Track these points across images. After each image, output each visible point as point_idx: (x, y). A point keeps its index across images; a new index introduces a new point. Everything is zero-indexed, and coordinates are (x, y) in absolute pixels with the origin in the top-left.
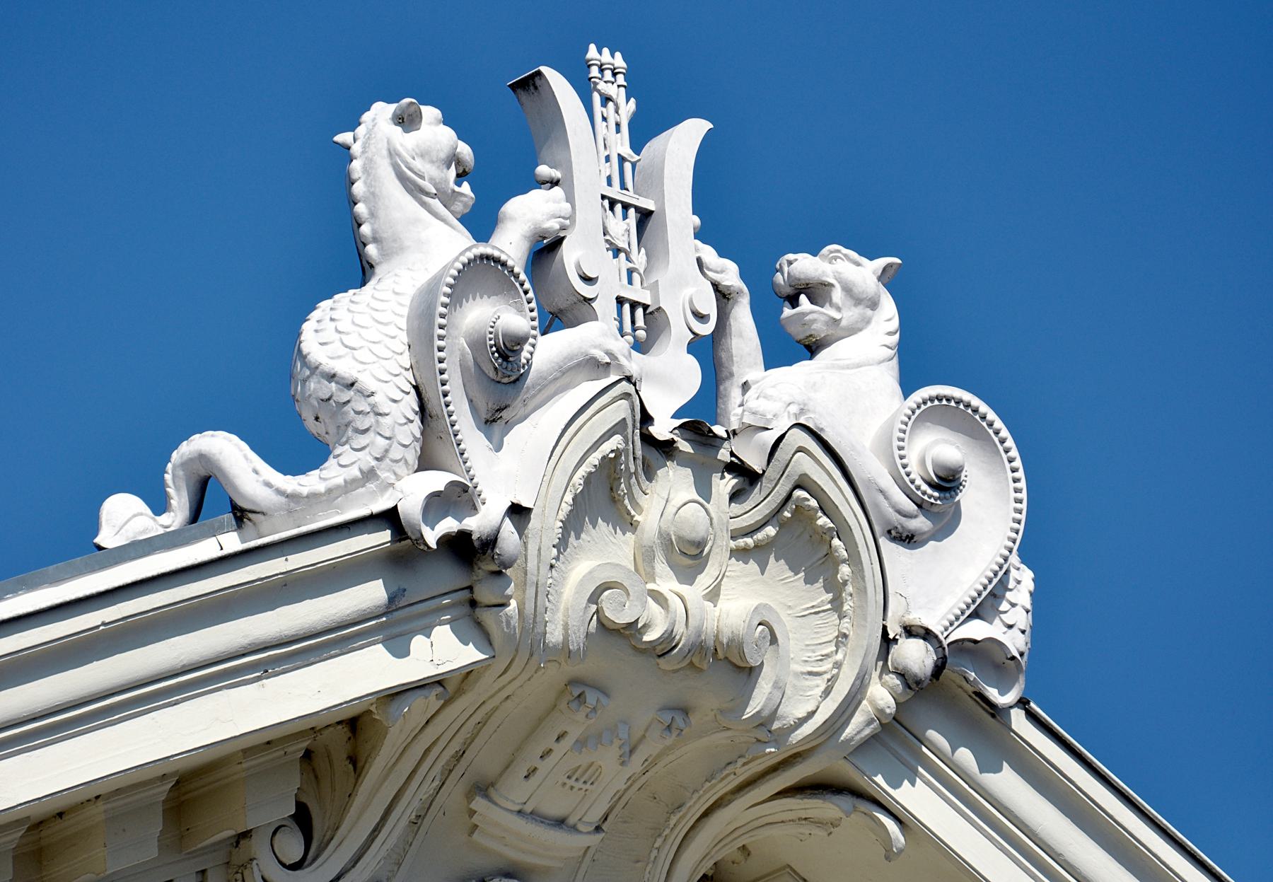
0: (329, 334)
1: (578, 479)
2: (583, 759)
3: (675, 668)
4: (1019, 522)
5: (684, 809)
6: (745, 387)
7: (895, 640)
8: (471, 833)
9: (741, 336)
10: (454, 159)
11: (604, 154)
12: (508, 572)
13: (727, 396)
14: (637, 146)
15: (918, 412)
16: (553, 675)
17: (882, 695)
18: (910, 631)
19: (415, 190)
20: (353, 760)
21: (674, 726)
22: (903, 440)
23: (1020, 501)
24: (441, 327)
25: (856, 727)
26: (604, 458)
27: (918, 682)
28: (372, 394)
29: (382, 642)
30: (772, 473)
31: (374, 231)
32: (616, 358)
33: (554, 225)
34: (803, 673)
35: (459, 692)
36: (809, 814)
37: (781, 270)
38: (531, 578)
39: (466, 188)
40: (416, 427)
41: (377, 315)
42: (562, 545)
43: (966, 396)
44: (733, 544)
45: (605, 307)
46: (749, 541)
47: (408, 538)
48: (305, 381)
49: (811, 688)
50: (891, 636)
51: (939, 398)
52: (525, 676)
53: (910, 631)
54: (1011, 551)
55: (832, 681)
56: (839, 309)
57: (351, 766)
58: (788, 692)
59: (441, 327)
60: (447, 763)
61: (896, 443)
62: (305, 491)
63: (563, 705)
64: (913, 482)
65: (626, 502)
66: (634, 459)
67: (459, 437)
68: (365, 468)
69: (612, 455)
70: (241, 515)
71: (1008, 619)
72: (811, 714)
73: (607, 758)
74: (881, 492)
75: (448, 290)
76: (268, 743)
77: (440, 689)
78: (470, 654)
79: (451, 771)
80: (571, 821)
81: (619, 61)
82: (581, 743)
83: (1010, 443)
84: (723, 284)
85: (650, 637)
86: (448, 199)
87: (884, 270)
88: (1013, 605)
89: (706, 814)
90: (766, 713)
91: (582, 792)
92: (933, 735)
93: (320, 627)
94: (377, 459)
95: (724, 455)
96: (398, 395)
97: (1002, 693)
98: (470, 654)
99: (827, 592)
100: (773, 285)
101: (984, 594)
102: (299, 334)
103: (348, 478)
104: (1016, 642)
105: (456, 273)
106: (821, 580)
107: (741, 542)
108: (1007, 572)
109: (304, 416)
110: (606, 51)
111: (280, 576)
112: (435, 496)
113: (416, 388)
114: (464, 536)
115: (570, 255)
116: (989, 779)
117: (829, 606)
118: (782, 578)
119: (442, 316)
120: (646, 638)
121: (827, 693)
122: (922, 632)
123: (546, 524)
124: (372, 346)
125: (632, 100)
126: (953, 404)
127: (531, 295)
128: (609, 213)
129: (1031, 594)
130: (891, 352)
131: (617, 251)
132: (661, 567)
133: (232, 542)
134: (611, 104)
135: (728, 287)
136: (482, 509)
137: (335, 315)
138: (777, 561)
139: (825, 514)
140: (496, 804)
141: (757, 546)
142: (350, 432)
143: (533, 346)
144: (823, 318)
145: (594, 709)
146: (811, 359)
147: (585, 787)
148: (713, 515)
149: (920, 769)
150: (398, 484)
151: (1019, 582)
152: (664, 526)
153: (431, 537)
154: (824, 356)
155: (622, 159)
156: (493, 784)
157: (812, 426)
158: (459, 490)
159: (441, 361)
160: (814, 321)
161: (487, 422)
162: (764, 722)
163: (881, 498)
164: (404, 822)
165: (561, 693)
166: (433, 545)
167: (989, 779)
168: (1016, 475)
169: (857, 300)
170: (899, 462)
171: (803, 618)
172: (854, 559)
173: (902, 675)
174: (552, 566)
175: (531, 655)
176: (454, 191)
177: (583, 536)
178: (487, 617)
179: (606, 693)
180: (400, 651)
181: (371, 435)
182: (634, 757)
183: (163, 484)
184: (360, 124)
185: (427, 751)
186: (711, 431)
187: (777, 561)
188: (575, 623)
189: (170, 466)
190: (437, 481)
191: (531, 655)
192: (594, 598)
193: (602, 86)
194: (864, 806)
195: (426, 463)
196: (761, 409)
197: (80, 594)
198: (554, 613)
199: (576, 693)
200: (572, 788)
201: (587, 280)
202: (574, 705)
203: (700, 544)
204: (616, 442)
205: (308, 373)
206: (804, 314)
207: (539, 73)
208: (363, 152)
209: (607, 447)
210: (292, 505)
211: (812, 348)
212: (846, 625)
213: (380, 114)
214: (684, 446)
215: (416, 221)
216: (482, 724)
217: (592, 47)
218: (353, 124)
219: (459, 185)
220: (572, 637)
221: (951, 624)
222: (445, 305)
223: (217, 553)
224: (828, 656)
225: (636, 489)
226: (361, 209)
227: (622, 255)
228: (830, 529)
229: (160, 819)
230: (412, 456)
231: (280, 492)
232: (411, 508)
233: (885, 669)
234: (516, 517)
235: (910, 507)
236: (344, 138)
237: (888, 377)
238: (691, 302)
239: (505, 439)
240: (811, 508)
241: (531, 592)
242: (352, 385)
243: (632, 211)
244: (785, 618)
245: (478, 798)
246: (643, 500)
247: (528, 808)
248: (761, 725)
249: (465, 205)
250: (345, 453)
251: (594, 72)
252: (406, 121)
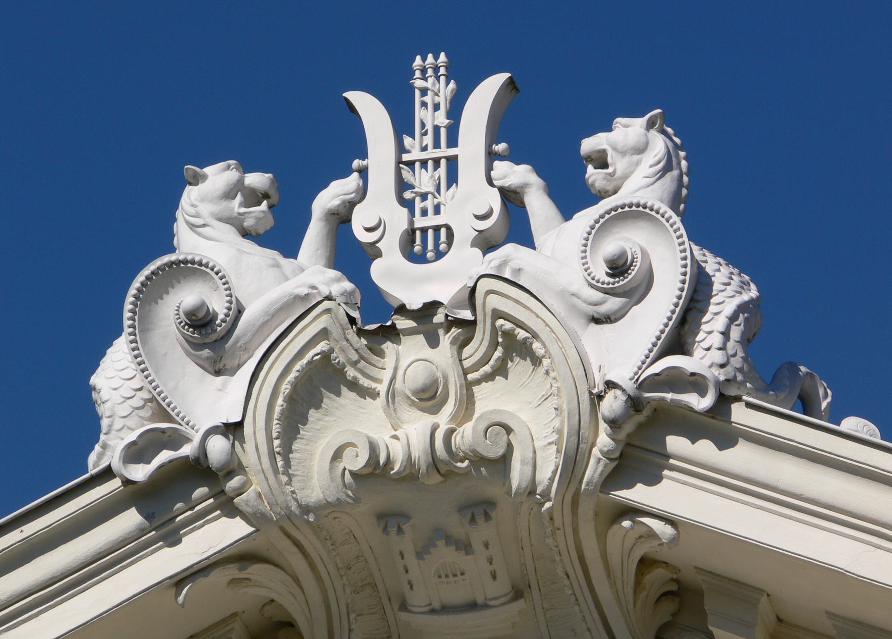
25: (594, 470)
30: (480, 317)
34: (545, 446)
74: (574, 295)
84: (506, 185)
111: (17, 544)
118: (521, 384)
163: (575, 299)
169: (622, 153)
171: (540, 406)
188: (324, 483)
235: (599, 296)
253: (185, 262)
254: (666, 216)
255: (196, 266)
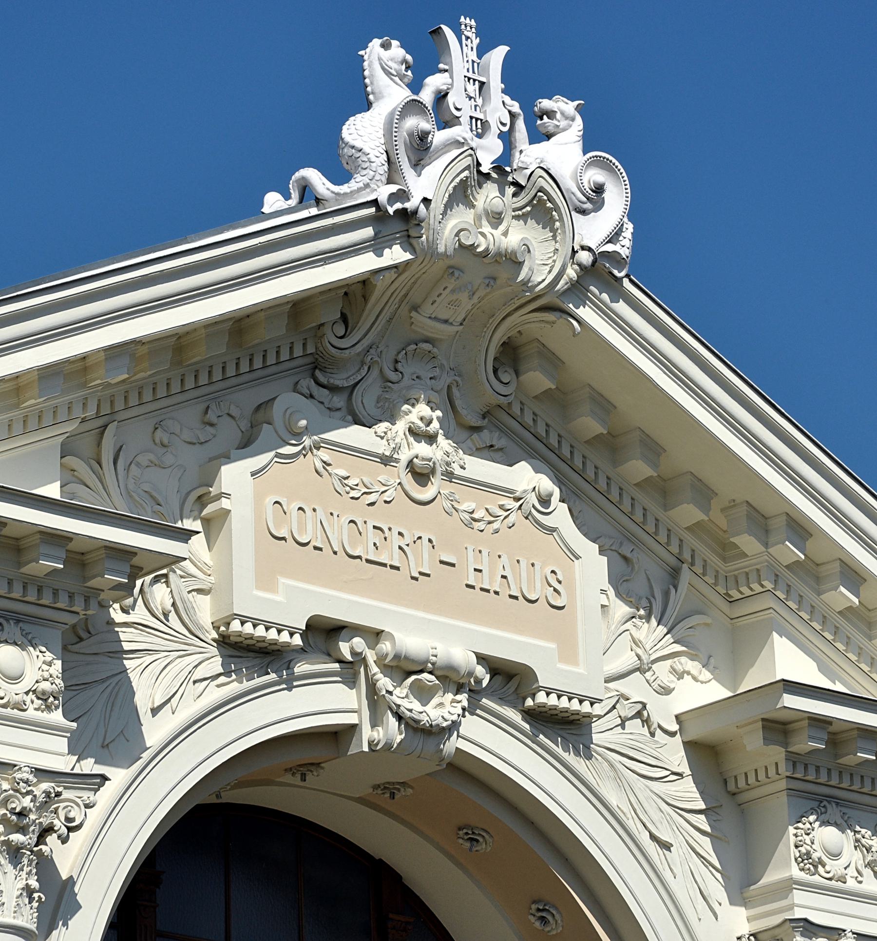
0: (352, 130)
1: (451, 188)
2: (454, 297)
3: (490, 262)
4: (627, 205)
5: (495, 317)
6: (521, 152)
7: (577, 252)
8: (411, 325)
9: (519, 131)
10: (404, 61)
11: (466, 59)
12: (423, 224)
13: (514, 155)
14: (480, 56)
15: (588, 162)
16: (441, 265)
17: (571, 273)
18: (583, 248)
19: (388, 74)
20: (364, 297)
21: (490, 285)
22: (581, 173)
23: (628, 197)
24: (396, 128)
25: (561, 285)
26: (461, 180)
27: (586, 268)
28: (368, 154)
29: (373, 251)
30: (529, 186)
31: (372, 90)
32: (467, 141)
33: (445, 87)
34: (541, 264)
35: (404, 271)
36: (544, 319)
37: (537, 106)
38: (432, 227)
39: (409, 73)
40: (386, 167)
41: (372, 123)
42: (444, 214)
43: (607, 156)
44: (513, 214)
45: (465, 120)
46: (520, 213)
47: (382, 211)
48: (343, 149)
49: (544, 270)
50: (575, 250)
51: (596, 157)
52: (429, 265)
53: (583, 248)
54: (623, 217)
55: (552, 267)
56: (559, 121)
57: (363, 299)
58: (535, 272)
59: (396, 128)
60: (401, 298)
61: (579, 174)
62: (342, 192)
63: (446, 276)
64: (585, 189)
65: (471, 197)
66: (474, 180)
67: (403, 171)
68: (365, 183)
69: (465, 179)
70: (318, 201)
71: (622, 243)
72: (544, 280)
73: (464, 297)
75: (399, 113)
76: (330, 290)
77: (396, 270)
78: (408, 256)
79: (403, 301)
80: (451, 321)
81: (473, 23)
82: (453, 291)
83: (624, 174)
85: (479, 250)
86: (402, 77)
87: (578, 106)
88: (625, 238)
89: (504, 319)
90: (525, 280)
91: (454, 310)
92: (592, 288)
93: (346, 245)
94: (370, 180)
95: (510, 179)
96: (379, 155)
97: (619, 272)
98: (408, 256)
99: (551, 232)
100: (534, 112)
101: (613, 234)
102: (342, 130)
103: (359, 187)
104: (625, 252)
105: (402, 107)
106: (548, 228)
107: (517, 213)
108: (622, 225)
109: (343, 162)
110: (468, 19)
112: (393, 194)
113: (386, 152)
114: (405, 210)
115: (451, 99)
116: (614, 305)
117: (551, 238)
119: (396, 123)
120: (478, 250)
121: (550, 272)
122: (588, 248)
123: (438, 206)
124: (369, 135)
125: (478, 38)
126: (602, 159)
127: (432, 115)
128: (468, 83)
129: (632, 233)
130: (579, 138)
131: (470, 98)
132: (485, 222)
133: (314, 211)
134: (469, 40)
135: (514, 112)
136: (412, 200)
137: (355, 123)
138: (531, 220)
139: (550, 202)
140: (420, 314)
141: (523, 214)
142: (360, 169)
143: (433, 135)
144: (552, 125)
145: (458, 278)
146: (548, 141)
147: (455, 308)
148: (505, 202)
149: (587, 302)
150: (378, 190)
151: (627, 229)
152: (486, 207)
153: (391, 210)
154: (553, 139)
155: (473, 62)
156: (419, 307)
157: (545, 167)
158: (402, 192)
159: (396, 141)
160: (549, 126)
161: (414, 165)
162: (525, 283)
163: (573, 196)
164: (384, 321)
165: (445, 271)
166: (392, 214)
167: (614, 305)
168: (626, 187)
170: (580, 182)
172: (561, 219)
173: (579, 265)
174: (440, 222)
175: (432, 256)
176: (404, 74)
177: (453, 210)
178: (414, 241)
179: (463, 272)
180: (380, 255)
181: (368, 170)
182: (474, 297)
183: (289, 189)
184: (367, 47)
185: (392, 294)
186: (504, 169)
187: (531, 220)
189: (291, 182)
190: (393, 188)
191: (432, 256)
192: (457, 235)
193: (466, 33)
194: (565, 316)
195: (390, 181)
196: (525, 161)
197: (250, 232)
198: (441, 240)
199: (451, 272)
200: (450, 308)
201: (458, 109)
202: (450, 276)
203: (500, 214)
204: (466, 173)
205: (344, 145)
206: (545, 123)
207: (440, 27)
208: (369, 58)
209: (462, 176)
210: (337, 197)
211: (549, 136)
212: (558, 246)
213: (376, 43)
214: (494, 175)
215: (389, 86)
216: (415, 283)
217: (462, 17)
218: (366, 47)
219: (407, 71)
220: (448, 250)
221: (599, 245)
222: (397, 119)
223: (309, 215)
224: (550, 257)
225: (475, 192)
226: (367, 81)
227: (473, 100)
228: (552, 208)
229: (286, 318)
230: (384, 179)
231: (333, 192)
232: (383, 198)
233: (573, 263)
234: (425, 203)
235: (585, 199)
236: (361, 53)
237: (579, 147)
238: (499, 118)
239: (422, 172)
240: (544, 200)
241: (431, 232)
242: (361, 150)
243: (477, 82)
244: (534, 243)
245: (413, 312)
246: (477, 196)
247: (433, 316)
248: (524, 284)
249: (409, 79)
250: (358, 178)
251: (463, 27)
252: (386, 46)
253: (419, 102)
254: (623, 175)
255: (614, 167)
